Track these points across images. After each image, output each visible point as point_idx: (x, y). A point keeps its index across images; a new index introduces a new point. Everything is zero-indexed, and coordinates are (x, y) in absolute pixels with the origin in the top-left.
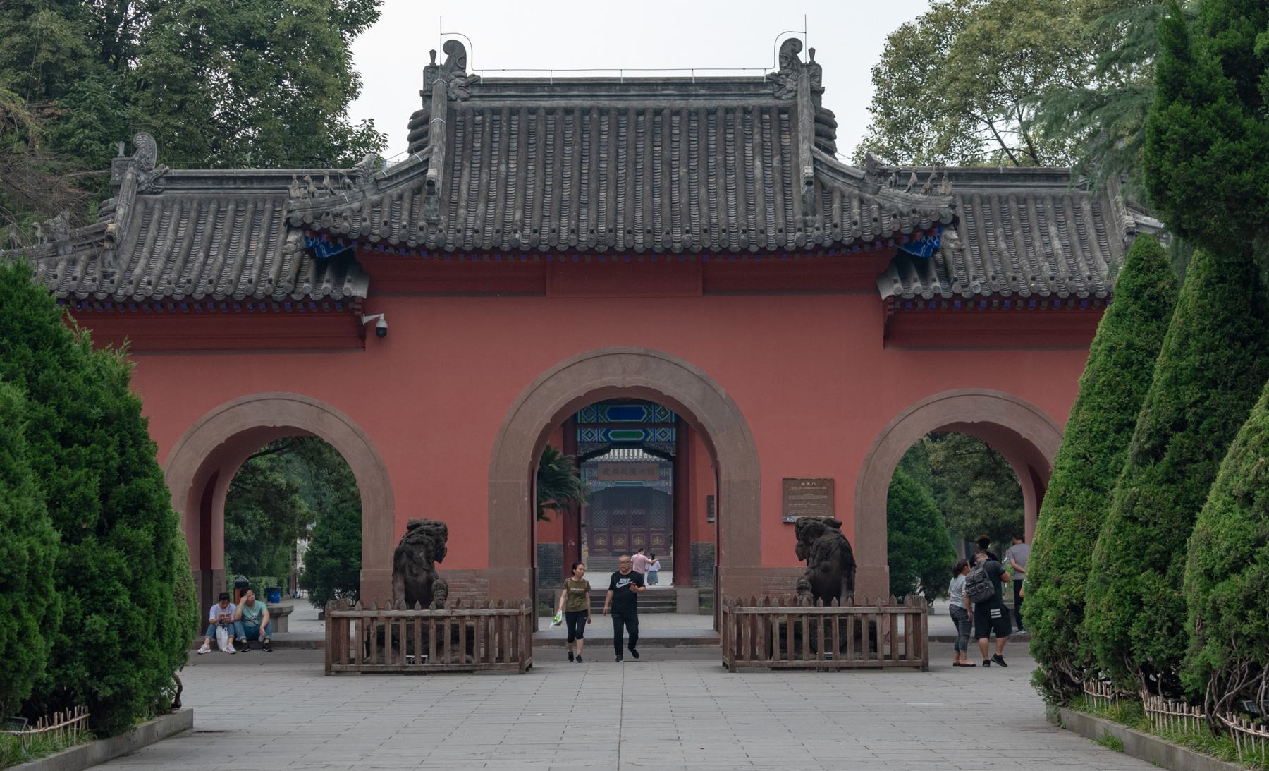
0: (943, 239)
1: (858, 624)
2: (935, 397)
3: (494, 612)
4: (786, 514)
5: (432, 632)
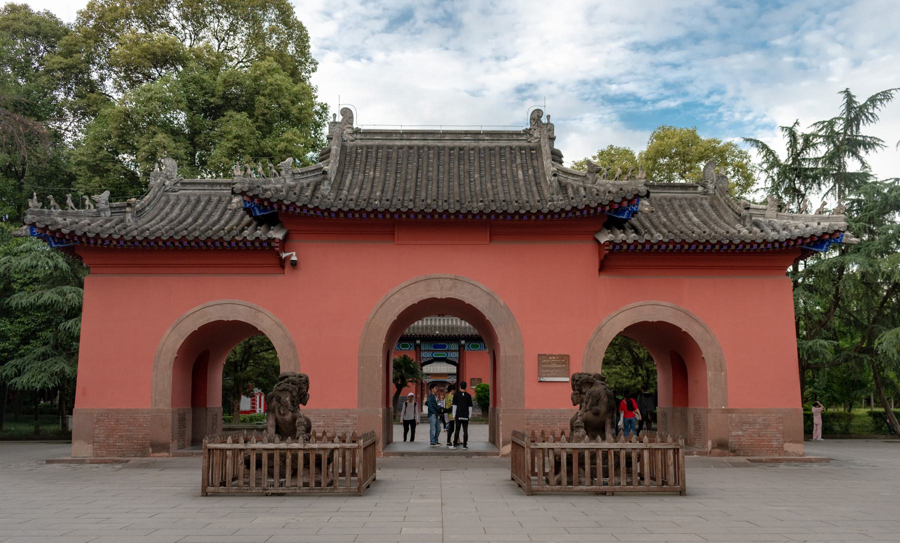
0: (640, 206)
1: (617, 455)
2: (631, 305)
3: (338, 445)
4: (540, 376)
5: (288, 461)
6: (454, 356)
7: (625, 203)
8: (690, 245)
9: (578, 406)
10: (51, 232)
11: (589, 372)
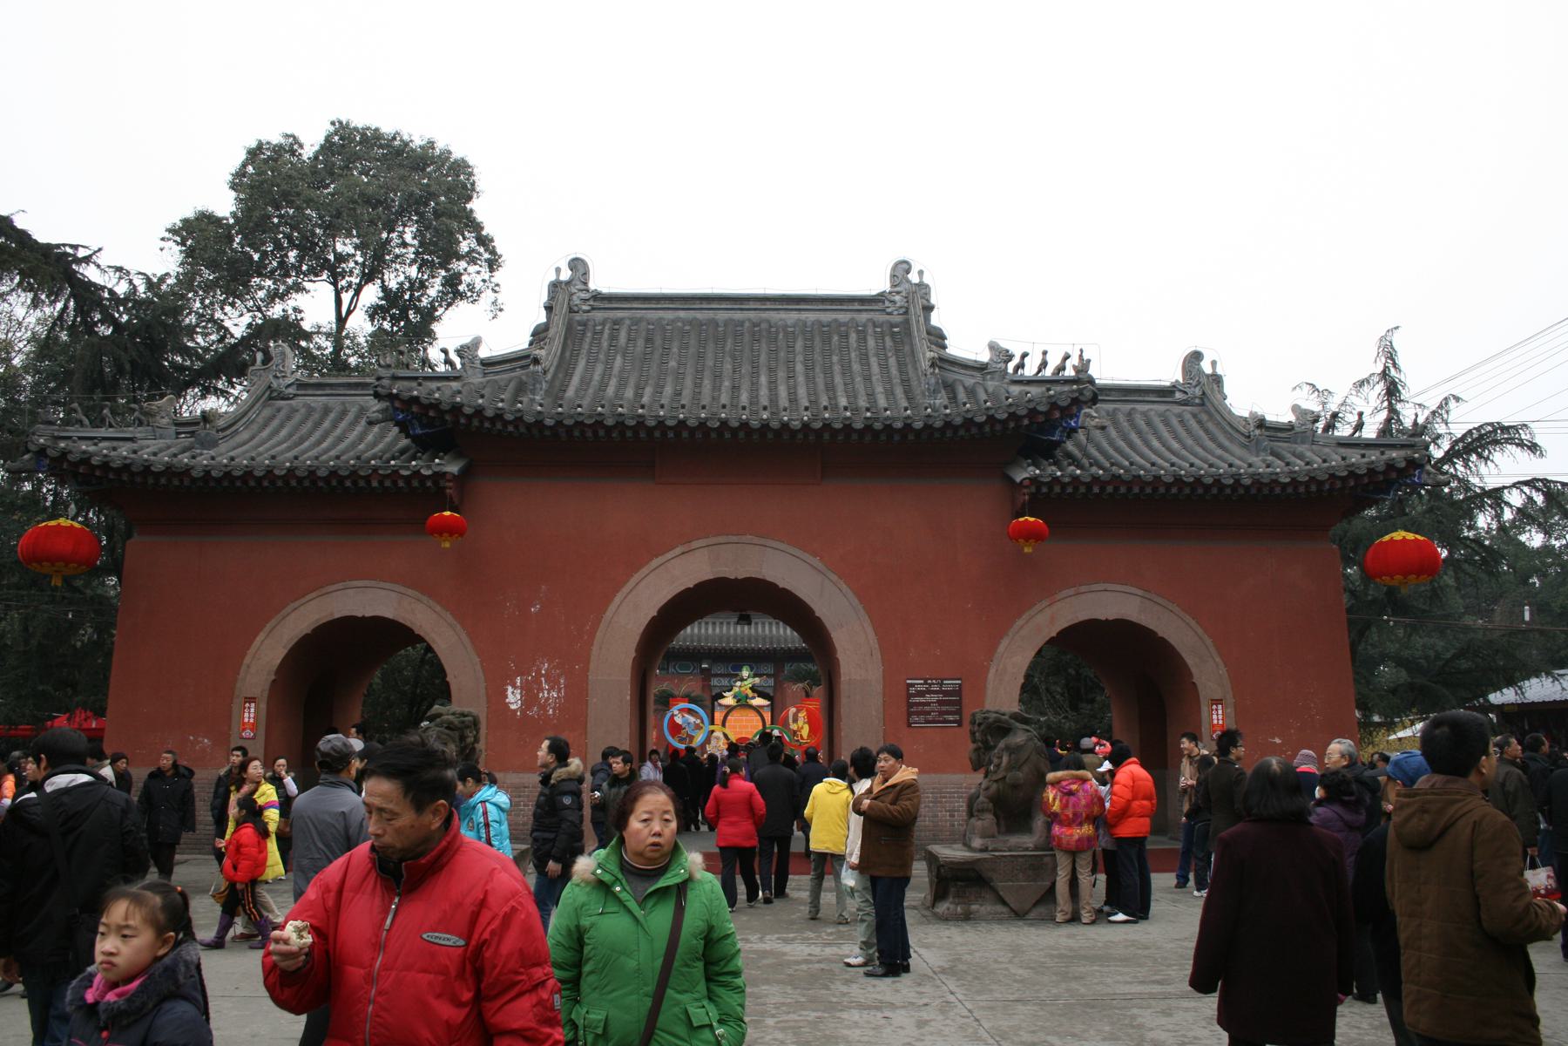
7: (1057, 414)
11: (1003, 710)
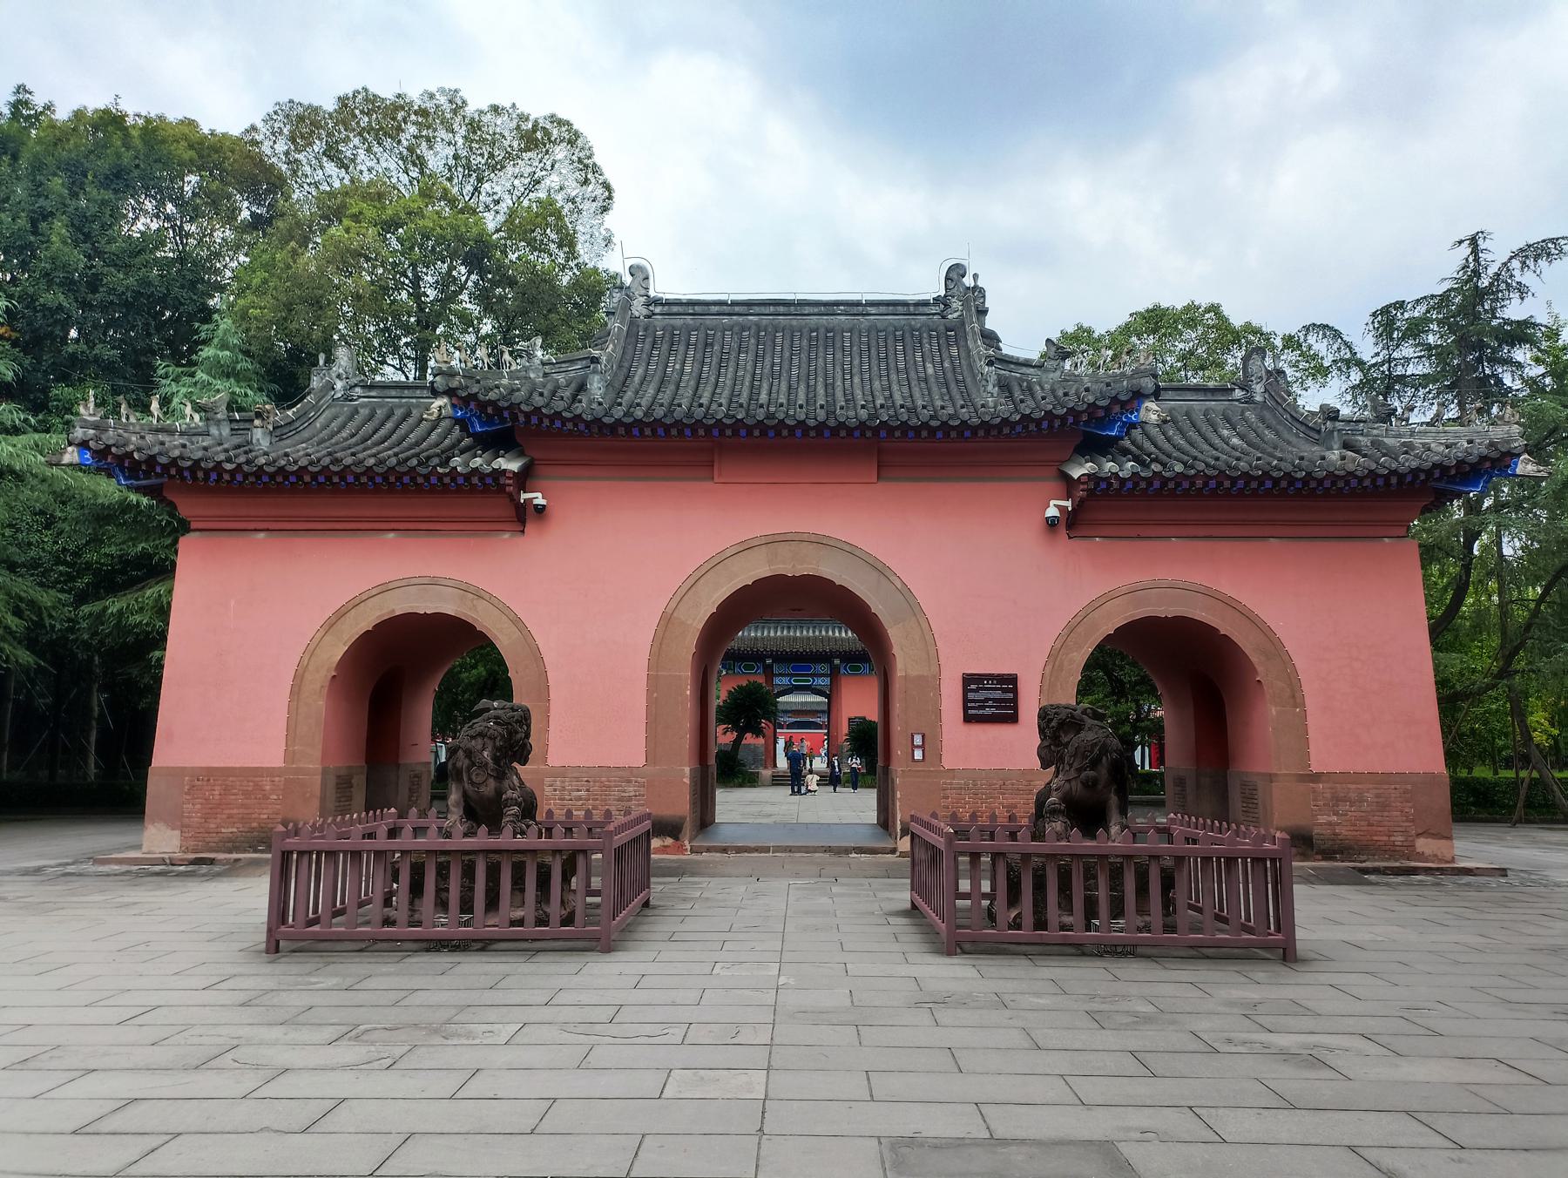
0: (1143, 411)
6: (823, 682)
8: (1234, 480)
9: (1053, 768)
10: (115, 456)
